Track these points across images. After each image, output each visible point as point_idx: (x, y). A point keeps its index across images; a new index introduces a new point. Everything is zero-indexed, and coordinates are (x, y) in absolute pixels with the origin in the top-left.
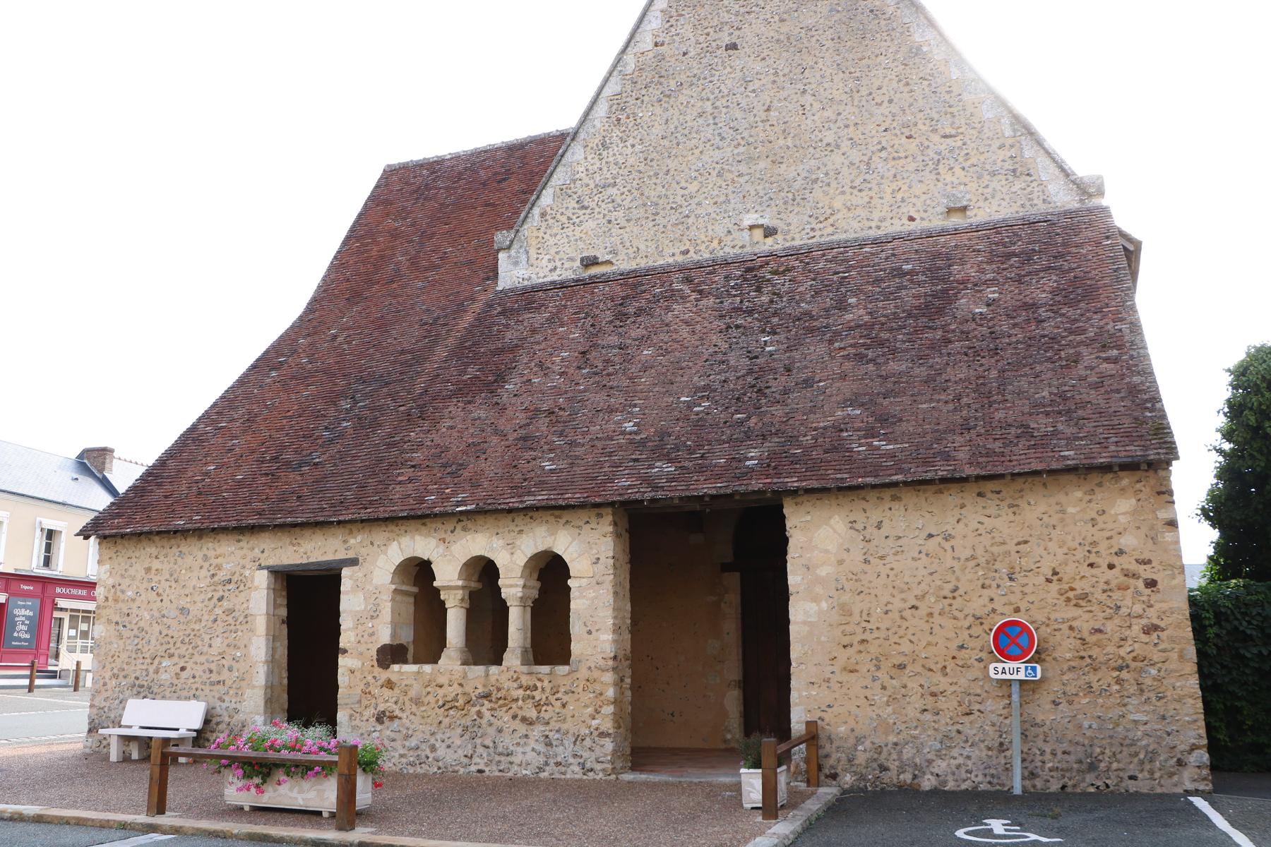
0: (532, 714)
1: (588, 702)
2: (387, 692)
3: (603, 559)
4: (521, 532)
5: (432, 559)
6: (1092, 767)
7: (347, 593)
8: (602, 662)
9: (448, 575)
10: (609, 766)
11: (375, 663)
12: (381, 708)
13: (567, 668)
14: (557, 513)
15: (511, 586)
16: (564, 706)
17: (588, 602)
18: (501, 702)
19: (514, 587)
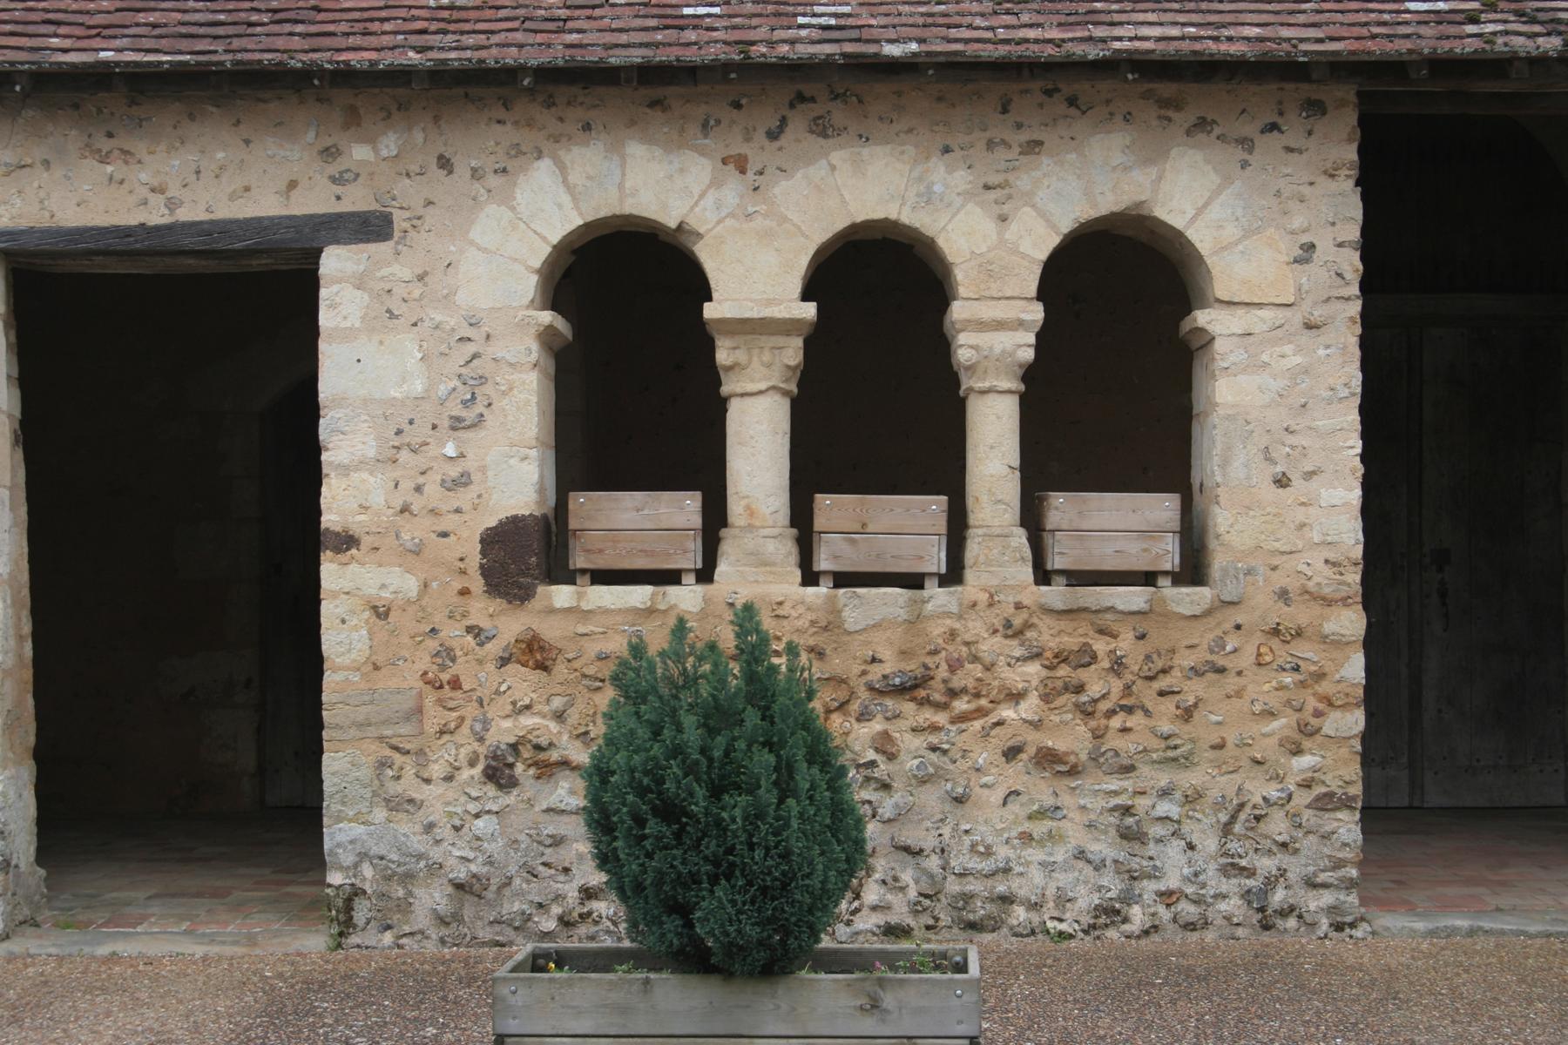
0: (1072, 739)
1: (1274, 702)
2: (521, 682)
3: (1325, 249)
4: (1033, 147)
5: (694, 223)
6: (474, 170)
7: (349, 335)
8: (1322, 577)
9: (756, 276)
10: (1354, 873)
11: (477, 584)
12: (504, 730)
13: (1204, 591)
14: (1167, 89)
15: (1000, 325)
16: (1187, 714)
17: (1277, 385)
18: (961, 705)
19: (995, 330)
